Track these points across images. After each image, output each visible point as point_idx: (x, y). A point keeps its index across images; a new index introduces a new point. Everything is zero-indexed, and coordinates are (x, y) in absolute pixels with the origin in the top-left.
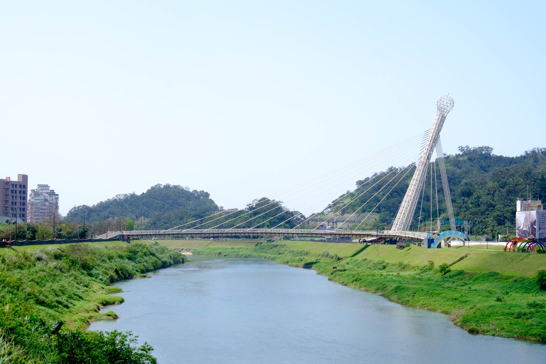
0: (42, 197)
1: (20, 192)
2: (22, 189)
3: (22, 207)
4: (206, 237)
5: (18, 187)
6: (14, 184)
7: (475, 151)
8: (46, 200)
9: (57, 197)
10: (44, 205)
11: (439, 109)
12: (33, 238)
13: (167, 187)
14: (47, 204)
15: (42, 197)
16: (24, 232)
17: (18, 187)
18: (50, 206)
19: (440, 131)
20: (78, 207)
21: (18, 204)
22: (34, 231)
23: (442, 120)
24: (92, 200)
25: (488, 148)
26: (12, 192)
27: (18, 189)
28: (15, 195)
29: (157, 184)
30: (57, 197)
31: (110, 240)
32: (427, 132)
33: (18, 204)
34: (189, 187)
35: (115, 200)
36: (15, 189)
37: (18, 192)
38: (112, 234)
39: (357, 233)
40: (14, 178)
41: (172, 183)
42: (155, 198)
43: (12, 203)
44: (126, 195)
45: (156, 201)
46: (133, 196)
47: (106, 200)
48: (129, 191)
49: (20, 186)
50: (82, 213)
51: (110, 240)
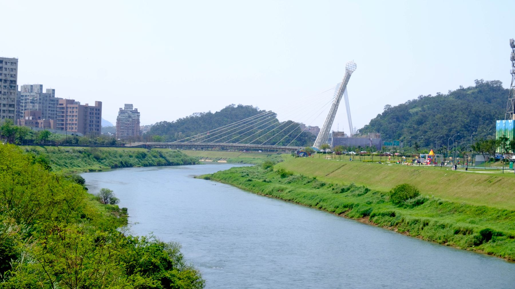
0: (126, 115)
1: (96, 114)
2: (98, 112)
3: (97, 124)
4: (241, 149)
5: (95, 110)
6: (92, 108)
7: (487, 84)
8: (130, 117)
9: (138, 114)
10: (128, 121)
11: (347, 69)
12: (77, 143)
13: (240, 107)
14: (130, 120)
15: (126, 115)
16: (71, 140)
17: (95, 110)
18: (133, 122)
19: (346, 84)
20: (160, 123)
21: (94, 122)
22: (77, 140)
23: (348, 77)
24: (172, 117)
25: (498, 82)
26: (90, 113)
27: (95, 112)
28: (92, 116)
29: (231, 104)
30: (138, 114)
31: (133, 147)
32: (338, 84)
33: (94, 122)
34: (259, 107)
35: (192, 118)
36: (92, 111)
37: (94, 114)
38: (137, 144)
39: (290, 147)
40: (92, 104)
41: (244, 104)
42: (225, 116)
43: (90, 121)
44: (201, 113)
45: (226, 119)
46: (209, 114)
47: (185, 117)
48: (206, 111)
49: (96, 110)
50: (164, 129)
51: (133, 147)
